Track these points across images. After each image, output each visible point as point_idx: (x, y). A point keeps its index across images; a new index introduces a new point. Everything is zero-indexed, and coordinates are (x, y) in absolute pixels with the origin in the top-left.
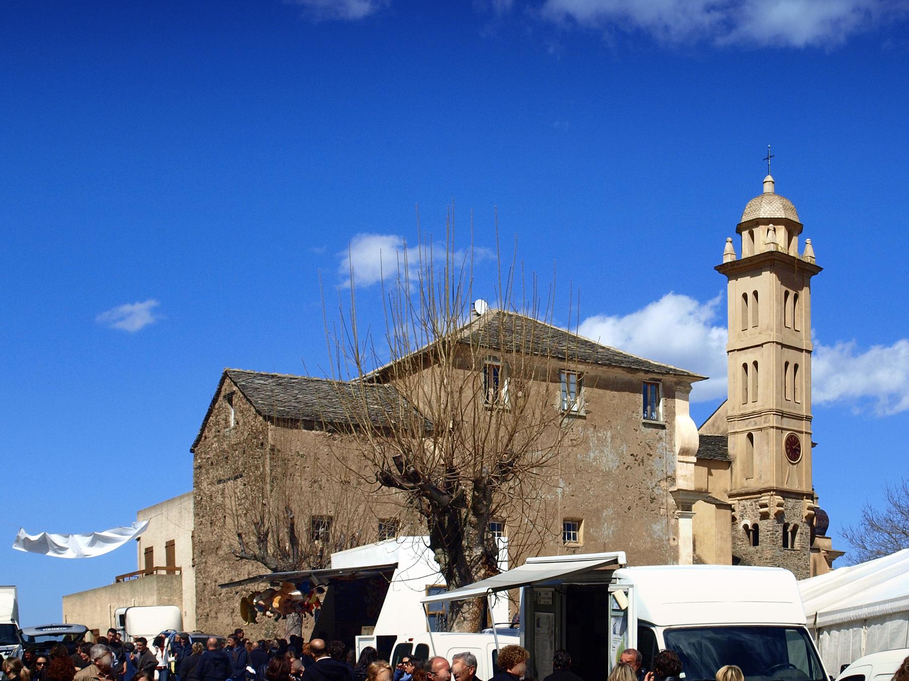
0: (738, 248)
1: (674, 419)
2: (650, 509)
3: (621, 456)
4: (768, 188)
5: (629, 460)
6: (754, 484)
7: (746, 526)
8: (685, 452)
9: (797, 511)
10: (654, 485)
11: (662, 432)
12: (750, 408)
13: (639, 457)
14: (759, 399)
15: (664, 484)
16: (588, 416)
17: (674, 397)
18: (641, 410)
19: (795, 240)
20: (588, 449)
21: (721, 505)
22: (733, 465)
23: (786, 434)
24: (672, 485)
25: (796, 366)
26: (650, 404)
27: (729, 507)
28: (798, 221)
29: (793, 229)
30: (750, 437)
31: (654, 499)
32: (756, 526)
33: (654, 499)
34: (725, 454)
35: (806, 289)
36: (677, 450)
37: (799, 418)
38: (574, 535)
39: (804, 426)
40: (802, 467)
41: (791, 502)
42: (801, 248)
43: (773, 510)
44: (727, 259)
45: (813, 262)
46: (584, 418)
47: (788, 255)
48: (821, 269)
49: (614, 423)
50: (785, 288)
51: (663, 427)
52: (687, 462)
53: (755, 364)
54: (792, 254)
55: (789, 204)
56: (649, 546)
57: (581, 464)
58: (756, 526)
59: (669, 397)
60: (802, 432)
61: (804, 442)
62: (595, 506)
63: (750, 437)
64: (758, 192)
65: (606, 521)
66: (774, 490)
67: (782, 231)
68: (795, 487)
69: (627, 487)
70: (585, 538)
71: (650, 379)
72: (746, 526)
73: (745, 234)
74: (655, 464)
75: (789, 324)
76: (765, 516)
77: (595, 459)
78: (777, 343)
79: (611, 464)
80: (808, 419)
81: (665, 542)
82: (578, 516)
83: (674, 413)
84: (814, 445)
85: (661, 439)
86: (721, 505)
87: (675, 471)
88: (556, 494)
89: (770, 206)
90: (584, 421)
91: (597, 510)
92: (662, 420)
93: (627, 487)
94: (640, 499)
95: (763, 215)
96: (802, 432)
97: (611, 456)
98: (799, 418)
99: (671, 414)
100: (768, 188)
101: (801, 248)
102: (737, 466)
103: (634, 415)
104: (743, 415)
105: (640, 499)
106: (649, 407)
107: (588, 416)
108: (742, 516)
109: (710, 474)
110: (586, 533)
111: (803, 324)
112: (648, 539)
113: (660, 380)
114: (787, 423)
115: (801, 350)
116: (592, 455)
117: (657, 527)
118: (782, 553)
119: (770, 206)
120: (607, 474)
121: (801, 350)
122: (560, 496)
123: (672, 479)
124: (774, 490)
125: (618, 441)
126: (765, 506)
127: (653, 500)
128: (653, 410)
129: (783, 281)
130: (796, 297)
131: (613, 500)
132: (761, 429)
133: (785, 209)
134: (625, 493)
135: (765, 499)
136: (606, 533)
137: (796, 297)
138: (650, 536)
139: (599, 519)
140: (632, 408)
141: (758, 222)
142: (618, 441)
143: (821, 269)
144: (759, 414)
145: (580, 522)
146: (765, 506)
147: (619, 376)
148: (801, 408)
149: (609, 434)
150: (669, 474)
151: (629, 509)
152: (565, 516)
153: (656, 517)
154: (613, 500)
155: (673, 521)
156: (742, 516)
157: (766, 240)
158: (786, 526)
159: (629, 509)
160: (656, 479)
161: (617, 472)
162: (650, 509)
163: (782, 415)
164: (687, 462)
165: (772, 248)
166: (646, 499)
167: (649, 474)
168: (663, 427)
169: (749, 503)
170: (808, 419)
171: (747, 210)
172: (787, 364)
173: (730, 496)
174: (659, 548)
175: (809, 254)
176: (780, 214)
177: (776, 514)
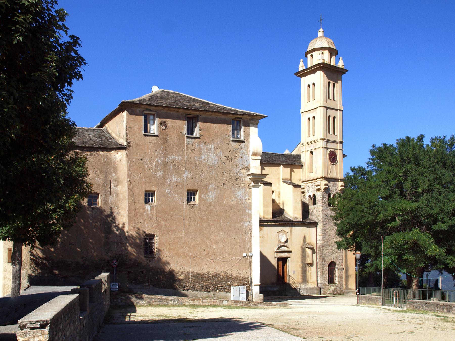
0: (305, 63)
1: (249, 138)
2: (235, 184)
3: (220, 157)
4: (320, 34)
5: (224, 159)
6: (313, 176)
7: (310, 196)
8: (255, 154)
9: (335, 188)
10: (238, 172)
11: (242, 145)
12: (312, 139)
13: (230, 158)
14: (316, 134)
15: (244, 171)
16: (201, 138)
17: (249, 126)
18: (231, 134)
19: (333, 58)
20: (201, 154)
21: (296, 186)
22: (304, 167)
23: (329, 150)
24: (247, 172)
25: (334, 118)
26: (236, 129)
27: (300, 186)
28: (335, 48)
29: (333, 52)
30: (312, 152)
31: (238, 179)
32: (314, 196)
33: (238, 179)
34: (300, 162)
35: (339, 82)
36: (251, 153)
37: (337, 142)
38: (194, 198)
39: (339, 146)
40: (338, 166)
41: (332, 184)
42: (337, 62)
43: (323, 187)
44: (300, 69)
45: (343, 67)
46: (199, 138)
47: (330, 65)
48: (347, 71)
49: (215, 141)
50: (328, 81)
51: (243, 142)
52: (256, 159)
53: (314, 117)
54: (332, 64)
55: (330, 41)
56: (235, 203)
57: (197, 162)
58: (314, 196)
59: (247, 126)
60: (337, 149)
61: (339, 154)
62: (205, 183)
63: (312, 152)
64: (316, 36)
65: (211, 190)
66: (323, 178)
67: (326, 53)
68: (334, 176)
69: (223, 173)
70: (199, 199)
71: (236, 118)
72: (310, 196)
73: (309, 56)
74: (238, 161)
75: (331, 97)
76: (318, 190)
77: (205, 159)
78: (324, 107)
79: (214, 162)
80: (341, 142)
81: (244, 201)
82: (195, 188)
83: (249, 135)
84: (344, 156)
85: (242, 148)
86: (296, 186)
87: (249, 164)
88: (183, 178)
89: (321, 41)
90: (199, 140)
91: (206, 185)
92: (242, 139)
93: (223, 173)
94: (230, 179)
95: (317, 47)
96: (337, 149)
97: (214, 158)
98: (337, 142)
99: (247, 135)
100: (320, 34)
101: (337, 62)
102: (306, 167)
103: (227, 136)
104: (308, 143)
105: (230, 179)
106: (235, 132)
107: (201, 138)
108: (308, 191)
109: (292, 171)
110: (200, 197)
111: (338, 97)
112: (235, 200)
113: (241, 118)
114: (330, 145)
115: (337, 110)
116: (203, 157)
117: (239, 193)
118: (327, 208)
119: (321, 41)
120: (212, 167)
121: (337, 110)
122: (185, 178)
123: (248, 168)
124: (323, 178)
125: (218, 150)
126: (319, 186)
127: (237, 179)
128: (238, 134)
129: (328, 77)
130: (334, 85)
131: (215, 180)
132: (316, 149)
133: (328, 43)
134: (222, 176)
135: (318, 182)
136: (211, 197)
137: (334, 85)
138: (235, 198)
139: (207, 189)
140: (226, 133)
141: (314, 50)
142: (218, 150)
143: (347, 71)
144: (315, 142)
145: (197, 191)
146: (319, 186)
147: (218, 117)
148: (337, 138)
149: (213, 146)
150: (246, 166)
151: (224, 184)
152: (188, 188)
153: (239, 187)
154: (215, 180)
155: (248, 190)
156: (308, 191)
157: (317, 58)
158: (329, 196)
159: (224, 184)
160: (239, 169)
161: (217, 165)
162: (235, 184)
163: (328, 141)
164: (256, 159)
165: (321, 61)
166: (233, 179)
167: (235, 166)
168: (243, 142)
169: (311, 184)
170: (341, 142)
171: (309, 46)
172: (329, 117)
173: (302, 182)
174: (241, 204)
175: (341, 64)
176: (326, 46)
177: (324, 189)
